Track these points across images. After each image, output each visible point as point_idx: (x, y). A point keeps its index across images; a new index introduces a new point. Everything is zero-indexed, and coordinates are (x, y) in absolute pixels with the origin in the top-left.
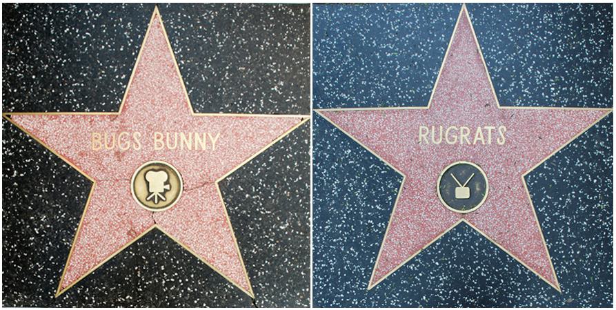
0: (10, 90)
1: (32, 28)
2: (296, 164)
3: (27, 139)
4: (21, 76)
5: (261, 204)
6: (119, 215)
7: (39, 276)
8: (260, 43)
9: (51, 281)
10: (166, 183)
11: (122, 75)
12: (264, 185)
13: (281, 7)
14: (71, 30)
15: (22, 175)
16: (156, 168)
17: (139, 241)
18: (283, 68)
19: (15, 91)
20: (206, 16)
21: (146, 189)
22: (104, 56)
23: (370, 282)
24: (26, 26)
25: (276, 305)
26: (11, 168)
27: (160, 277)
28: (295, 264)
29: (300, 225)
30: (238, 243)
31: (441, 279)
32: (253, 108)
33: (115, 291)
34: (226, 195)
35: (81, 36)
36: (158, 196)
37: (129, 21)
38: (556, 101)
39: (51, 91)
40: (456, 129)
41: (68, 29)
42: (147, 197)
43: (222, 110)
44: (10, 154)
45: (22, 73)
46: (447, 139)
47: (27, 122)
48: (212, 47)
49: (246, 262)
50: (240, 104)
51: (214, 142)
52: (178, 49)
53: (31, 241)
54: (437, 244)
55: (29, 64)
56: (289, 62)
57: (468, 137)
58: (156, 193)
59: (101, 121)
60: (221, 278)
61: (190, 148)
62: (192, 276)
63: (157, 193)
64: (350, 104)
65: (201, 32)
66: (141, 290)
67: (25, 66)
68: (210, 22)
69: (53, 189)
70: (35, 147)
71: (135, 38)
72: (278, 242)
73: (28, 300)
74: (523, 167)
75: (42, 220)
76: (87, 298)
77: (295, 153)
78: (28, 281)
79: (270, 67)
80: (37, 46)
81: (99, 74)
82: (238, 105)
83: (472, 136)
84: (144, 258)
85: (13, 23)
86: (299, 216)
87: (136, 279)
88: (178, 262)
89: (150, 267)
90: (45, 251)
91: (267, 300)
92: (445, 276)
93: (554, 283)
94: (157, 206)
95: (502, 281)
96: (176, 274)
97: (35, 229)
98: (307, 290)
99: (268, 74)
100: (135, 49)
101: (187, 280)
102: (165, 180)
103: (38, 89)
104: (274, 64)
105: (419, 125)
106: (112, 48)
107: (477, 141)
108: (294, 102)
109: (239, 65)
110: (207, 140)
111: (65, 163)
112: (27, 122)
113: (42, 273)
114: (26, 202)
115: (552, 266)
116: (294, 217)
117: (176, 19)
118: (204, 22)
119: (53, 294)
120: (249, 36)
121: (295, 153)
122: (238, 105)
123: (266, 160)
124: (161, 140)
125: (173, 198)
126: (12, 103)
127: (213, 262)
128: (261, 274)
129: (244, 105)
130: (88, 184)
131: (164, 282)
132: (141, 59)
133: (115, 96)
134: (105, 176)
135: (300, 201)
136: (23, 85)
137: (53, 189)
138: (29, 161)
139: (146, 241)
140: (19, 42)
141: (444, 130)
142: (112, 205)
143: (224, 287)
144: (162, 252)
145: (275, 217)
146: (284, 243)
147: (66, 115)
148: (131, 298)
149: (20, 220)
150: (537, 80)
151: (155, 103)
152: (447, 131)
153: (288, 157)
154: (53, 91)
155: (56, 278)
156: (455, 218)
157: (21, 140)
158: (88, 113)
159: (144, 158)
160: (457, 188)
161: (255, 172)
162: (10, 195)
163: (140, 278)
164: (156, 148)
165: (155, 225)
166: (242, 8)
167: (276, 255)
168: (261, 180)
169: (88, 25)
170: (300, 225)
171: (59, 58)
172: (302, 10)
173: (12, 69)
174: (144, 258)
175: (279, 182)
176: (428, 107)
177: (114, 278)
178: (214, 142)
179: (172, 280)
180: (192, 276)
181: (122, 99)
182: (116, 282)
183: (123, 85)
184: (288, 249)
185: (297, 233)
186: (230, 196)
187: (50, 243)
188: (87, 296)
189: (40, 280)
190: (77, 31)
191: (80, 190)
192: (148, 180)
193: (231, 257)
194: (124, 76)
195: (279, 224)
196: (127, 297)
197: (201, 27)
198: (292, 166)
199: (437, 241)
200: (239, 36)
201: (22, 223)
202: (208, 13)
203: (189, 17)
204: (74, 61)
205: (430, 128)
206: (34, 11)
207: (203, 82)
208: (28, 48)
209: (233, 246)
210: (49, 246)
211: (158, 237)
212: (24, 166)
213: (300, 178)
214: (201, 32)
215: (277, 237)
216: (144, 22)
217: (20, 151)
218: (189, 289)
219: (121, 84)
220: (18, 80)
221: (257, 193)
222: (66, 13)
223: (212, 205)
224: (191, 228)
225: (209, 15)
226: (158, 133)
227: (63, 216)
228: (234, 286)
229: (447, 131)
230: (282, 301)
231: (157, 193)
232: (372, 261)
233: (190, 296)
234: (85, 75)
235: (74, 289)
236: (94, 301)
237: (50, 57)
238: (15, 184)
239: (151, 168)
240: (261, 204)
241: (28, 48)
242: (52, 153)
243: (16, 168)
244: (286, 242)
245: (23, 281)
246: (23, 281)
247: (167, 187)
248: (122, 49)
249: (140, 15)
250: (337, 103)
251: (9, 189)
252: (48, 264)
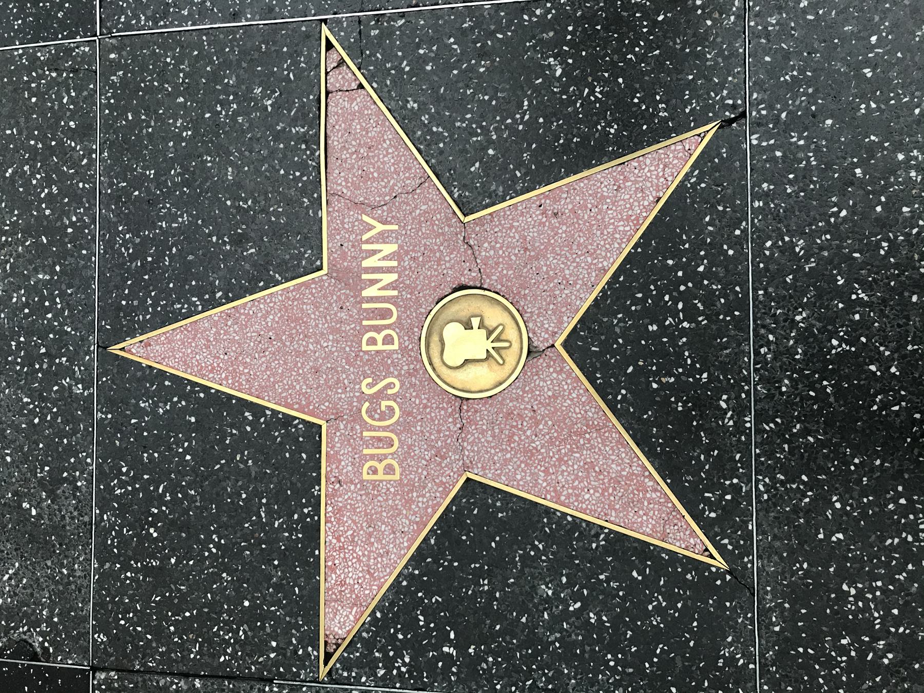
0: (272, 655)
1: (146, 605)
2: (421, 52)
3: (374, 621)
4: (245, 632)
5: (509, 121)
6: (537, 423)
7: (679, 605)
8: (178, 138)
9: (689, 576)
10: (468, 326)
11: (246, 418)
12: (469, 116)
13: (108, 99)
14: (152, 525)
15: (452, 636)
17: (592, 381)
18: (226, 89)
20: (127, 249)
22: (204, 457)
24: (142, 618)
26: (436, 659)
27: (674, 333)
28: (640, 36)
29: (551, 34)
32: (307, 148)
33: (710, 432)
34: (490, 197)
35: (166, 504)
37: (137, 404)
39: (275, 567)
41: (152, 530)
43: (315, 213)
44: (407, 660)
45: (238, 629)
48: (189, 234)
49: (638, 146)
50: (302, 175)
51: (380, 227)
52: (194, 303)
53: (599, 619)
55: (220, 614)
56: (215, 77)
58: (489, 345)
59: (340, 461)
62: (670, 262)
65: (159, 258)
66: (705, 375)
67: (224, 621)
68: (138, 240)
69: (482, 567)
70: (392, 604)
71: (171, 392)
72: (590, 79)
75: (550, 592)
76: (728, 497)
77: (400, 54)
78: (691, 631)
79: (227, 115)
80: (183, 596)
81: (242, 466)
82: (305, 178)
84: (630, 369)
85: (136, 647)
86: (534, 37)
87: (679, 389)
88: (640, 295)
89: (652, 355)
90: (620, 588)
91: (725, 92)
96: (667, 298)
97: (571, 609)
99: (240, 119)
101: (680, 274)
102: (460, 327)
103: (271, 595)
104: (219, 109)
106: (189, 440)
108: (296, 63)
109: (223, 179)
110: (377, 242)
111: (426, 540)
113: (672, 599)
114: (511, 629)
116: (534, 46)
117: (134, 309)
118: (140, 253)
119: (720, 574)
120: (165, 160)
121: (400, 54)
122: (305, 178)
123: (415, 115)
124: (380, 337)
126: (300, 652)
127: (637, 219)
128: (665, 110)
129: (303, 167)
131: (686, 325)
132: (212, 380)
133: (288, 433)
134: (455, 453)
135: (500, 36)
136: (263, 627)
137: (482, 567)
138: (421, 618)
139: (593, 365)
140: (174, 633)
142: (516, 438)
143: (695, 190)
144: (617, 330)
145: (536, 89)
146: (593, 63)
148: (725, 397)
149: (553, 643)
151: (302, 349)
153: (407, 69)
154: (276, 562)
155: (682, 565)
157: (376, 634)
158: (324, 489)
159: (415, 370)
161: (438, 137)
162: (495, 663)
163: (678, 377)
164: (396, 346)
165: (558, 345)
166: (110, 177)
167: (620, 80)
168: (458, 124)
169: (144, 489)
170: (551, 34)
171: (209, 550)
172: (112, 56)
173: (229, 651)
174: (630, 369)
175: (460, 85)
176: (325, 271)
177: (674, 438)
178: (380, 227)
179: (680, 306)
180: (670, 262)
181: (296, 418)
182: (690, 432)
183: (266, 416)
184: (607, 55)
185: (569, 37)
186: (493, 188)
187: (602, 577)
188: (722, 497)
189: (689, 603)
190: (156, 511)
191: (484, 507)
193: (626, 179)
194: (247, 414)
195: (550, 80)
196: (724, 405)
197: (150, 259)
198: (425, 60)
200: (166, 181)
201: (556, 640)
202: (121, 245)
203: (129, 282)
204: (215, 519)
205: (366, 458)
206: (112, 601)
207: (258, 253)
208: (187, 614)
209: (600, 177)
210: (608, 580)
211: (582, 339)
212: (433, 630)
213: (452, 40)
214: (159, 258)
215: (580, 82)
216: (139, 374)
217: (400, 636)
218: (701, 269)
219: (262, 420)
220: (253, 637)
221: (486, 131)
222: (119, 534)
223: (512, 227)
224: (563, 270)
225: (125, 243)
227: (541, 546)
228: (694, 167)
230: (725, 58)
233: (717, 266)
234: (244, 496)
235: (706, 526)
236: (735, 481)
237: (208, 568)
238: (471, 650)
240: (509, 121)
241: (187, 614)
242: (406, 567)
243: (438, 647)
244: (592, 60)
245: (692, 644)
246: (692, 644)
248: (193, 419)
251: (484, 666)
252: (650, 582)
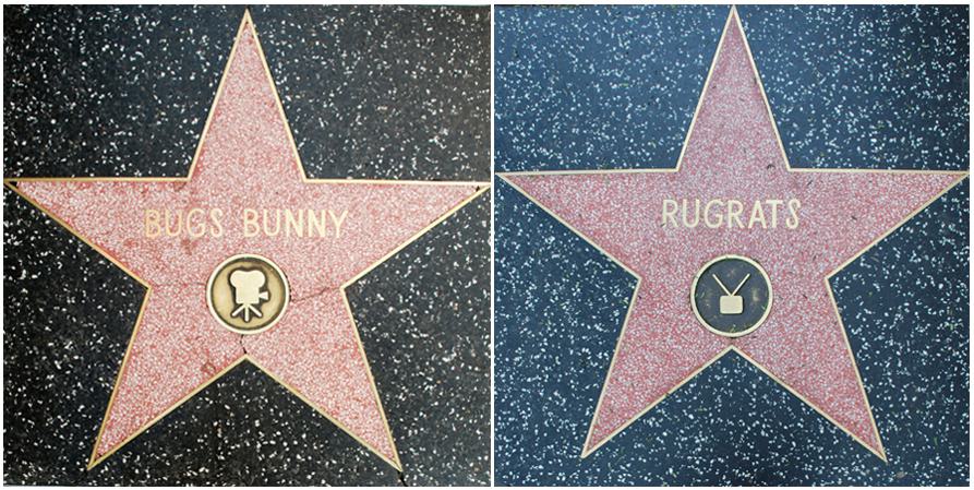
0: (16, 142)
1: (51, 44)
2: (468, 259)
3: (43, 219)
4: (32, 121)
5: (413, 323)
6: (188, 340)
7: (62, 437)
8: (411, 68)
9: (81, 443)
10: (263, 289)
11: (193, 119)
12: (418, 293)
13: (444, 12)
14: (112, 47)
15: (34, 277)
16: (247, 265)
17: (220, 380)
18: (448, 107)
20: (325, 25)
21: (230, 298)
22: (164, 88)
23: (586, 445)
24: (41, 41)
25: (437, 482)
26: (17, 265)
27: (253, 437)
28: (467, 417)
29: (474, 355)
30: (376, 385)
31: (697, 441)
32: (400, 170)
33: (182, 460)
34: (358, 308)
35: (128, 57)
36: (250, 310)
37: (204, 34)
38: (879, 160)
39: (81, 144)
40: (722, 204)
41: (107, 46)
42: (233, 312)
43: (350, 174)
44: (16, 243)
45: (34, 116)
46: (706, 220)
47: (43, 193)
48: (335, 75)
49: (389, 415)
50: (379, 165)
51: (338, 224)
52: (282, 78)
53: (49, 382)
54: (692, 386)
55: (45, 101)
56: (457, 99)
57: (740, 217)
58: (247, 306)
59: (160, 192)
60: (349, 440)
61: (300, 234)
62: (304, 436)
63: (249, 306)
64: (553, 165)
65: (318, 51)
66: (223, 458)
67: (40, 104)
68: (332, 34)
69: (83, 299)
70: (55, 232)
71: (214, 60)
72: (439, 382)
73: (44, 474)
75: (67, 347)
76: (137, 471)
77: (467, 243)
78: (44, 443)
79: (427, 107)
80: (58, 73)
81: (156, 116)
82: (377, 167)
83: (747, 215)
84: (227, 407)
85: (20, 37)
86: (472, 342)
87: (215, 441)
88: (281, 414)
89: (238, 423)
90: (72, 396)
91: (422, 475)
92: (703, 437)
93: (876, 448)
94: (248, 326)
95: (794, 444)
96: (279, 433)
97: (56, 362)
99: (424, 117)
101: (296, 443)
102: (261, 285)
103: (60, 140)
104: (433, 101)
105: (663, 198)
106: (177, 75)
107: (755, 223)
108: (465, 162)
109: (378, 103)
110: (327, 221)
111: (102, 257)
112: (43, 193)
113: (66, 431)
114: (41, 320)
116: (465, 342)
117: (278, 30)
118: (322, 35)
119: (83, 464)
120: (394, 57)
121: (467, 243)
122: (377, 167)
123: (421, 253)
124: (254, 222)
125: (273, 314)
126: (19, 164)
127: (337, 414)
128: (413, 434)
129: (386, 165)
130: (140, 291)
131: (259, 446)
132: (223, 93)
133: (182, 152)
134: (166, 279)
135: (475, 318)
136: (36, 135)
137: (83, 299)
138: (46, 254)
139: (231, 381)
140: (31, 66)
141: (703, 205)
142: (177, 324)
143: (355, 454)
144: (256, 399)
145: (435, 343)
146: (449, 385)
147: (104, 182)
148: (207, 471)
149: (32, 349)
150: (850, 126)
151: (246, 162)
152: (707, 208)
153: (456, 248)
154: (84, 144)
155: (89, 439)
156: (719, 345)
157: (34, 221)
158: (139, 179)
159: (228, 250)
160: (723, 298)
161: (403, 271)
162: (17, 308)
163: (221, 439)
164: (247, 235)
165: (246, 356)
166: (382, 13)
167: (436, 404)
168: (412, 285)
169: (139, 40)
170: (474, 355)
171: (93, 92)
172: (477, 16)
173: (19, 109)
174: (227, 407)
175: (442, 287)
176: (677, 170)
177: (180, 439)
178: (338, 224)
179: (273, 442)
180: (304, 436)
181: (193, 157)
182: (183, 446)
183: (195, 134)
184: (456, 394)
185: (470, 368)
186: (364, 310)
187: (79, 384)
188: (138, 467)
189: (64, 443)
190: (122, 50)
191: (127, 300)
192: (233, 284)
193: (365, 406)
194: (196, 120)
195: (440, 354)
196: (201, 470)
197: (317, 43)
198: (462, 262)
199: (691, 382)
200: (378, 57)
201: (34, 352)
202: (329, 21)
203: (299, 27)
204: (117, 97)
205: (680, 202)
206: (53, 17)
207: (320, 130)
208: (45, 76)
209: (368, 388)
210: (77, 388)
211: (250, 375)
212: (38, 262)
213: (475, 282)
214: (318, 51)
215: (438, 375)
216: (228, 35)
217: (32, 238)
218: (299, 457)
219: (192, 132)
220: (28, 127)
221: (406, 306)
222: (104, 21)
223: (335, 324)
224: (301, 360)
225: (330, 24)
226: (250, 210)
227: (99, 341)
228: (371, 453)
229: (707, 208)
230: (445, 476)
231: (249, 306)
232: (588, 413)
233: (300, 467)
234: (134, 118)
235: (116, 456)
236: (148, 476)
237: (79, 91)
238: (24, 290)
239: (238, 265)
240: (413, 323)
241: (45, 76)
242: (83, 242)
243: (26, 265)
244: (452, 383)
245: (36, 444)
246: (36, 444)
247: (265, 295)
248: (192, 78)
249: (221, 24)
250: (533, 163)
251: (14, 299)
252: (76, 417)
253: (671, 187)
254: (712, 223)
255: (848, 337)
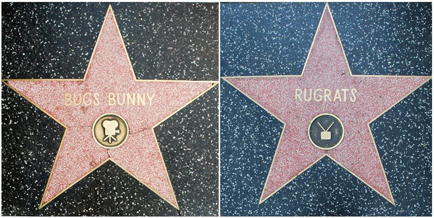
0: (7, 63)
1: (23, 20)
2: (208, 115)
3: (19, 98)
4: (14, 54)
5: (184, 144)
6: (84, 151)
7: (27, 194)
8: (183, 30)
9: (36, 197)
10: (117, 129)
11: (86, 53)
12: (186, 130)
13: (198, 5)
14: (50, 21)
15: (15, 123)
16: (110, 118)
17: (98, 169)
18: (199, 48)
19: (11, 64)
20: (145, 11)
21: (103, 133)
22: (73, 39)
23: (261, 198)
24: (18, 18)
26: (8, 118)
27: (113, 195)
28: (208, 185)
29: (211, 158)
30: (168, 171)
31: (311, 196)
32: (178, 76)
33: (81, 204)
34: (159, 137)
35: (57, 25)
36: (112, 138)
37: (91, 15)
38: (392, 71)
39: (36, 64)
41: (48, 21)
42: (104, 139)
43: (156, 78)
44: (7, 108)
45: (15, 51)
46: (315, 98)
47: (19, 86)
48: (149, 33)
49: (173, 185)
50: (169, 73)
51: (151, 100)
52: (126, 35)
53: (22, 170)
54: (308, 172)
55: (20, 45)
56: (204, 44)
58: (110, 136)
59: (71, 85)
60: (156, 196)
61: (134, 104)
62: (135, 194)
63: (111, 136)
64: (246, 73)
65: (142, 23)
66: (99, 204)
67: (18, 46)
68: (148, 15)
69: (37, 133)
70: (25, 103)
71: (95, 27)
72: (196, 170)
74: (368, 118)
75: (30, 155)
76: (61, 210)
77: (208, 108)
78: (20, 197)
79: (190, 47)
80: (26, 32)
81: (70, 52)
82: (168, 74)
84: (101, 181)
85: (9, 16)
86: (210, 152)
87: (96, 196)
88: (125, 184)
89: (106, 188)
90: (32, 176)
91: (188, 211)
92: (313, 194)
93: (390, 199)
94: (110, 145)
95: (354, 197)
96: (124, 193)
97: (25, 161)
98: (217, 204)
99: (189, 52)
100: (95, 34)
101: (132, 197)
102: (116, 127)
103: (27, 62)
104: (193, 45)
105: (295, 88)
106: (79, 33)
107: (336, 99)
108: (207, 72)
109: (169, 46)
110: (146, 99)
111: (46, 114)
112: (19, 86)
113: (29, 192)
114: (18, 142)
115: (389, 187)
116: (207, 152)
117: (124, 13)
118: (143, 16)
119: (37, 207)
120: (176, 25)
121: (208, 108)
122: (168, 74)
123: (188, 112)
124: (113, 99)
125: (122, 140)
126: (8, 73)
127: (150, 184)
128: (184, 193)
129: (172, 74)
130: (62, 129)
131: (115, 198)
132: (99, 42)
133: (81, 68)
134: (74, 124)
135: (212, 141)
136: (16, 60)
137: (37, 133)
138: (21, 113)
139: (103, 169)
140: (14, 29)
141: (313, 91)
142: (79, 144)
143: (158, 202)
144: (114, 177)
145: (194, 153)
146: (200, 171)
148: (92, 209)
149: (14, 155)
150: (379, 56)
151: (110, 72)
152: (315, 92)
153: (203, 110)
154: (37, 64)
155: (40, 196)
156: (320, 153)
157: (15, 98)
158: (62, 80)
159: (102, 111)
161: (180, 121)
162: (7, 137)
163: (99, 196)
164: (110, 104)
165: (110, 159)
166: (170, 6)
167: (194, 180)
168: (184, 127)
169: (62, 18)
170: (211, 158)
171: (41, 41)
172: (213, 7)
173: (8, 49)
174: (101, 181)
175: (197, 128)
176: (302, 75)
177: (80, 195)
178: (151, 100)
179: (121, 197)
180: (135, 194)
181: (86, 70)
182: (82, 199)
183: (87, 60)
184: (203, 175)
185: (210, 164)
186: (162, 138)
187: (35, 171)
188: (61, 208)
189: (28, 197)
190: (54, 22)
191: (56, 134)
192: (104, 126)
193: (163, 181)
194: (87, 53)
195: (196, 158)
196: (90, 209)
197: (141, 19)
198: (206, 116)
199: (308, 170)
200: (168, 25)
201: (15, 156)
202: (146, 9)
203: (133, 12)
204: (52, 43)
205: (303, 90)
206: (24, 8)
207: (143, 58)
208: (20, 34)
209: (164, 173)
210: (34, 173)
211: (111, 167)
212: (17, 117)
213: (212, 125)
214: (142, 23)
215: (195, 167)
216: (102, 16)
217: (14, 106)
218: (133, 203)
219: (85, 59)
220: (13, 57)
221: (181, 136)
222: (47, 9)
223: (149, 144)
224: (134, 160)
225: (147, 11)
226: (111, 93)
227: (44, 152)
228: (165, 201)
229: (315, 92)
230: (198, 212)
231: (111, 136)
232: (262, 184)
233: (134, 208)
234: (60, 53)
235: (52, 203)
236: (66, 212)
237: (35, 40)
238: (11, 129)
239: (106, 118)
240: (184, 144)
241: (20, 34)
242: (37, 108)
243: (11, 118)
244: (202, 170)
245: (16, 198)
246: (16, 198)
247: (118, 131)
248: (86, 35)
250: (237, 73)
251: (6, 133)
252: (34, 186)
253: (299, 83)
254: (317, 99)
255: (378, 150)
